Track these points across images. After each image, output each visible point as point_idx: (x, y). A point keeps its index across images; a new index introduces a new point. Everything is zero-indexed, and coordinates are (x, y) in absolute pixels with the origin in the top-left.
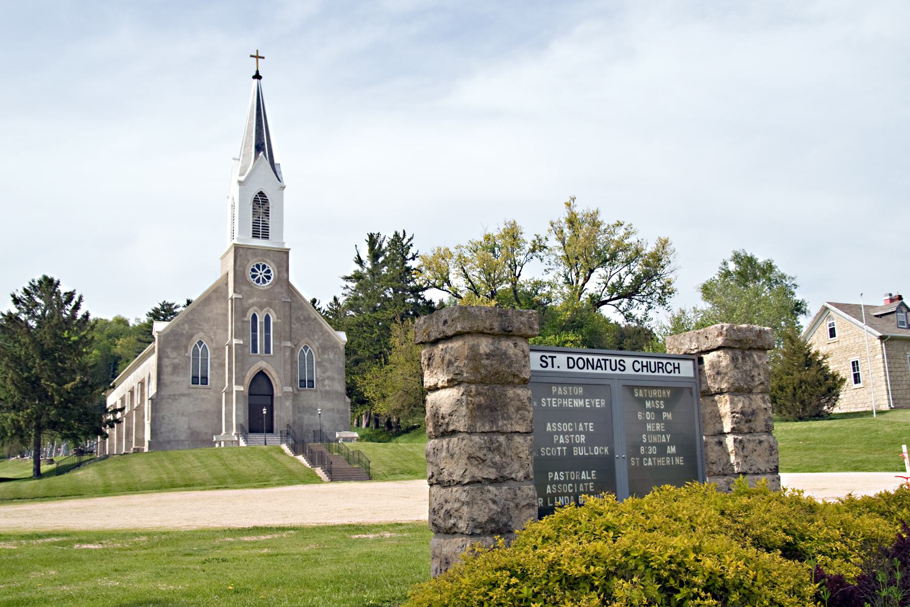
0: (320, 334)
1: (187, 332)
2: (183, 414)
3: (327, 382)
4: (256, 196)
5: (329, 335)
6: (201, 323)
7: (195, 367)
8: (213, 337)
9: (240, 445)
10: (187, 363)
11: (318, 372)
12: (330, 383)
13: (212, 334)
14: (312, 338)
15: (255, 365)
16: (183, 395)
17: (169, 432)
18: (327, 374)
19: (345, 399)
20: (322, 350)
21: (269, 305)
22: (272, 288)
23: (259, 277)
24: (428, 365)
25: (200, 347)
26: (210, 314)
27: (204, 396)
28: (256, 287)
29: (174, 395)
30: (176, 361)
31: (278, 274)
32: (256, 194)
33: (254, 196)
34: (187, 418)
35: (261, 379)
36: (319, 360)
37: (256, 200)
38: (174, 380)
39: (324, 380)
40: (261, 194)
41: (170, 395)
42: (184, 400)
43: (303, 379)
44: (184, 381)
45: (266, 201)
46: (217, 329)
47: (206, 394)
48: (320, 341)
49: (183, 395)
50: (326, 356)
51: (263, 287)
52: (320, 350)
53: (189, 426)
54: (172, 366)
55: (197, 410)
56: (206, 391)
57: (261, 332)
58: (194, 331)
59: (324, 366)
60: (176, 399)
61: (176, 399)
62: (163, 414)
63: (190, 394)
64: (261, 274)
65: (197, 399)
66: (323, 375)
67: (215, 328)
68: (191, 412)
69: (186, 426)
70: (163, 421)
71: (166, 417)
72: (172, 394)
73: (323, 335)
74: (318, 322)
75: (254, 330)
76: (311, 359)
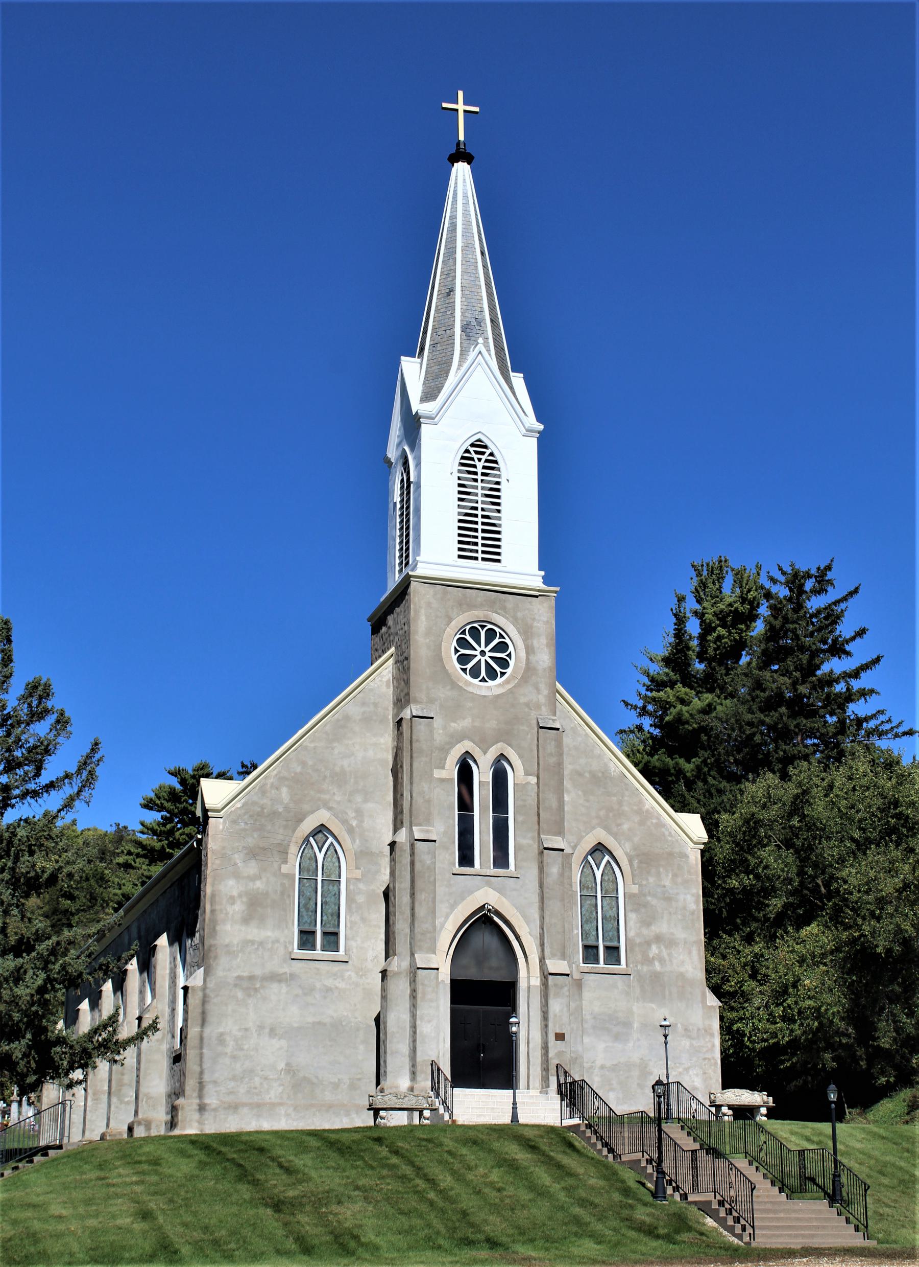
0: (637, 819)
1: (286, 808)
2: (273, 1032)
3: (654, 950)
4: (467, 451)
5: (661, 825)
6: (325, 786)
7: (588, 919)
8: (354, 823)
9: (201, 779)
10: (285, 893)
11: (631, 924)
12: (665, 953)
13: (352, 814)
14: (615, 829)
15: (469, 898)
16: (275, 978)
17: (234, 1078)
18: (655, 929)
19: (704, 995)
20: (640, 862)
21: (505, 735)
22: (511, 691)
23: (486, 645)
24: (310, 899)
25: (320, 851)
26: (345, 763)
27: (329, 982)
28: (470, 689)
29: (251, 978)
30: (259, 885)
31: (527, 653)
32: (467, 445)
33: (461, 453)
34: (283, 1043)
35: (484, 939)
36: (635, 889)
37: (466, 461)
38: (250, 937)
39: (648, 944)
40: (479, 446)
41: (239, 978)
42: (276, 991)
43: (591, 942)
44: (277, 941)
45: (492, 464)
46: (366, 801)
47: (335, 976)
48: (636, 839)
49: (275, 978)
50: (651, 880)
51: (489, 688)
52: (636, 862)
53: (288, 1064)
54: (245, 899)
55: (310, 1019)
56: (337, 967)
57: (483, 809)
58: (306, 807)
59: (646, 905)
60: (256, 990)
61: (256, 990)
62: (221, 1030)
63: (293, 976)
64: (483, 653)
65: (312, 989)
66: (645, 931)
67: (359, 798)
68: (296, 1025)
69: (281, 1065)
70: (220, 1048)
71: (228, 1038)
72: (246, 974)
73: (642, 823)
74: (628, 786)
75: (465, 805)
76: (611, 886)
